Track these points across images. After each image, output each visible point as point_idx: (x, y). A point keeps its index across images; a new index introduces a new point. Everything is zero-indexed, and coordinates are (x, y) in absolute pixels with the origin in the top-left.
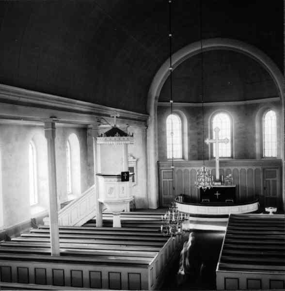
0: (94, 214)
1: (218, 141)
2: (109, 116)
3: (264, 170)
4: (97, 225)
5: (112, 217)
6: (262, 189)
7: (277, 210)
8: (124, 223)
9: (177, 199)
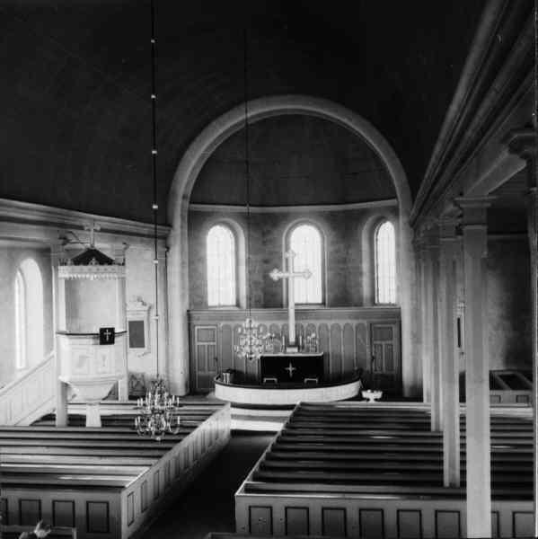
0: (52, 404)
2: (81, 228)
4: (57, 423)
7: (383, 395)
8: (106, 420)
9: (220, 377)
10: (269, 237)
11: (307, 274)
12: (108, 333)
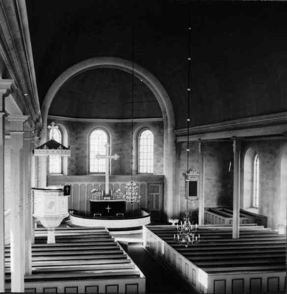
3: (148, 184)
5: (47, 233)
6: (146, 203)
11: (99, 157)
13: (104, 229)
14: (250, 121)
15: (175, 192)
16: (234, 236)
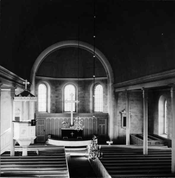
1: (72, 101)
5: (22, 149)
10: (57, 89)
12: (34, 122)
13: (63, 147)
14: (150, 77)
15: (115, 123)
16: (144, 153)
